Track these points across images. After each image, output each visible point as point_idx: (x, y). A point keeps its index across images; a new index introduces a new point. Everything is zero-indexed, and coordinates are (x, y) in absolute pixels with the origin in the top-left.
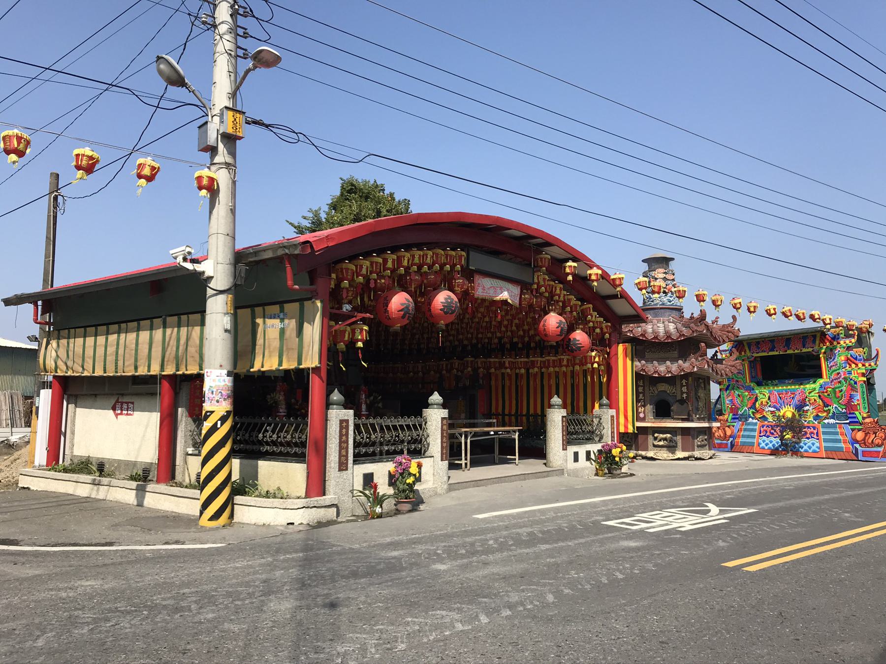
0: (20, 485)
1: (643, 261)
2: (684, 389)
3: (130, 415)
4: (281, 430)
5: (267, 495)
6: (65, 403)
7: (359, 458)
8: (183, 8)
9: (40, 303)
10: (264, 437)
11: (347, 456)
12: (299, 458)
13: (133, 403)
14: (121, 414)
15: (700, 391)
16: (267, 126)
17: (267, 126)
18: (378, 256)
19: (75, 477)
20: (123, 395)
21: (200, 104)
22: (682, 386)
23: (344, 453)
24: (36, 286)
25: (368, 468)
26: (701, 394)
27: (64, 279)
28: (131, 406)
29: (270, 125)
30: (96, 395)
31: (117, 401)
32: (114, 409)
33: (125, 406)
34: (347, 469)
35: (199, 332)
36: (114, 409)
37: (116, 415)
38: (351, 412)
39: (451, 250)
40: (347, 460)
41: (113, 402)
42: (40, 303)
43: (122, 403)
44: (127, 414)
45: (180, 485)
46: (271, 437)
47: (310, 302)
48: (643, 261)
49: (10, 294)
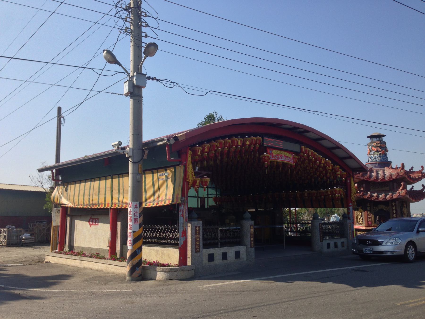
0: (46, 260)
1: (368, 137)
2: (394, 208)
3: (98, 225)
4: (174, 232)
5: (78, 254)
6: (68, 219)
7: (206, 246)
8: (116, 26)
9: (54, 170)
10: (173, 236)
11: (199, 245)
12: (174, 245)
13: (98, 219)
14: (93, 225)
15: (404, 209)
16: (158, 80)
17: (158, 80)
18: (229, 139)
19: (266, 281)
20: (93, 215)
21: (124, 71)
22: (392, 206)
23: (198, 243)
24: (52, 162)
25: (211, 251)
26: (405, 210)
27: (64, 159)
28: (97, 220)
29: (159, 80)
30: (81, 215)
31: (91, 218)
32: (89, 221)
33: (94, 220)
34: (199, 252)
35: (182, 171)
36: (89, 221)
37: (90, 225)
38: (201, 222)
39: (254, 136)
40: (199, 246)
41: (89, 218)
42: (54, 170)
43: (93, 219)
44: (95, 225)
45: (82, 254)
46: (169, 235)
47: (179, 166)
48: (368, 137)
49: (41, 167)
